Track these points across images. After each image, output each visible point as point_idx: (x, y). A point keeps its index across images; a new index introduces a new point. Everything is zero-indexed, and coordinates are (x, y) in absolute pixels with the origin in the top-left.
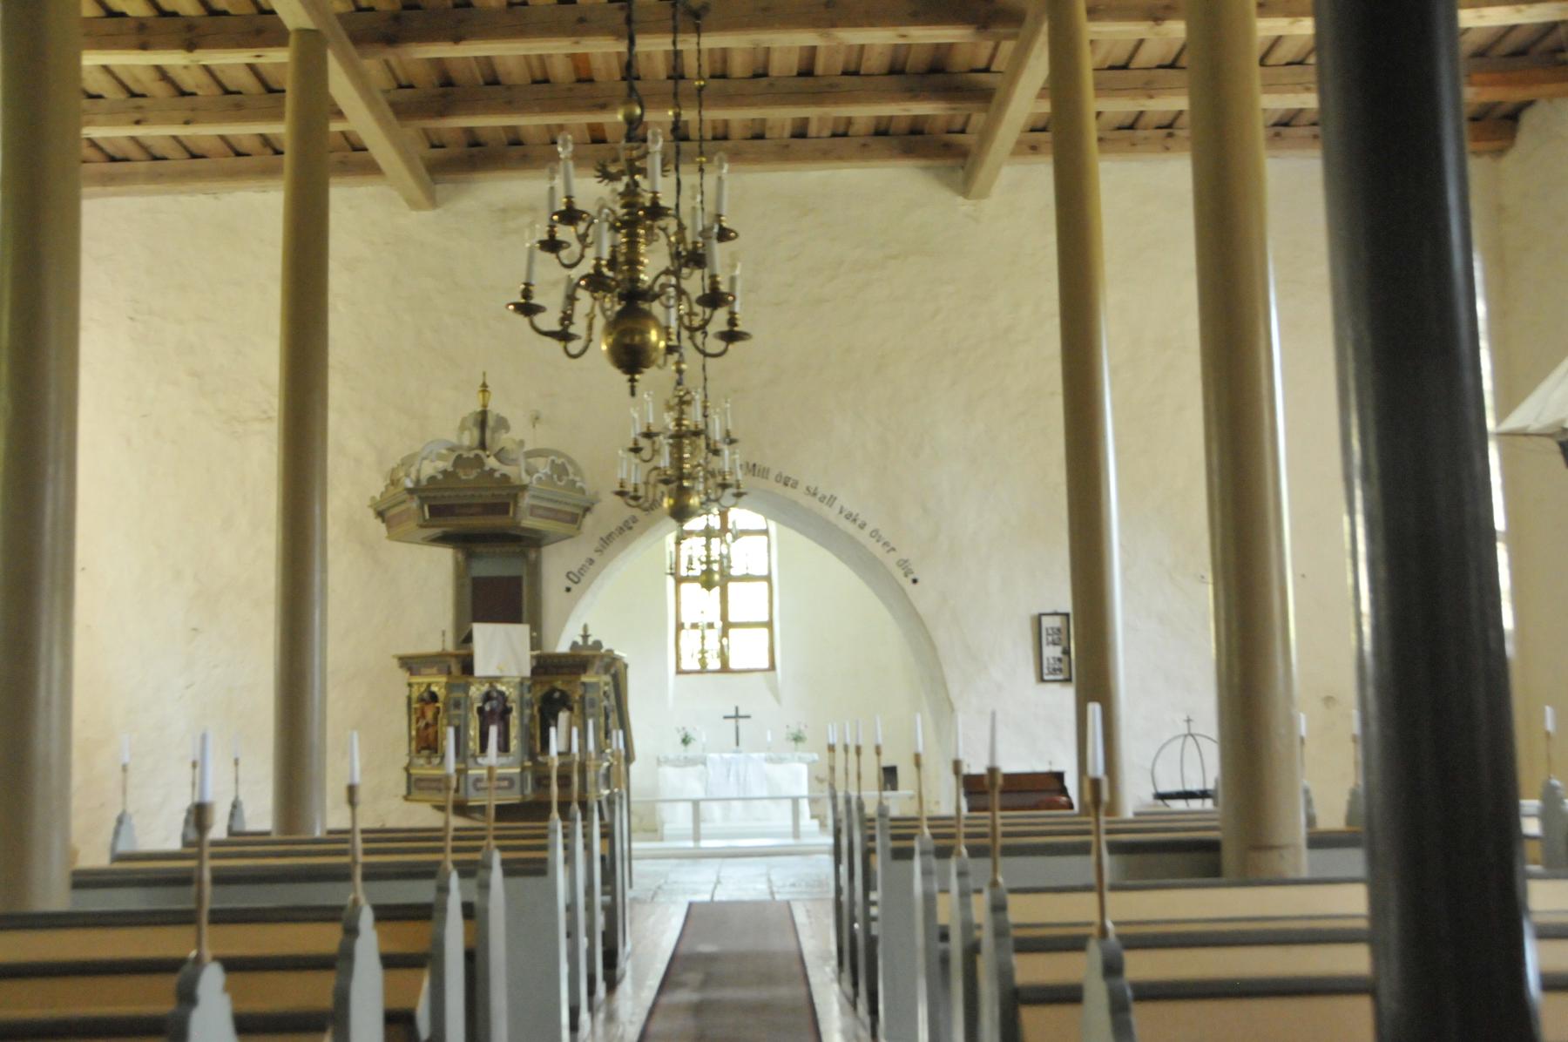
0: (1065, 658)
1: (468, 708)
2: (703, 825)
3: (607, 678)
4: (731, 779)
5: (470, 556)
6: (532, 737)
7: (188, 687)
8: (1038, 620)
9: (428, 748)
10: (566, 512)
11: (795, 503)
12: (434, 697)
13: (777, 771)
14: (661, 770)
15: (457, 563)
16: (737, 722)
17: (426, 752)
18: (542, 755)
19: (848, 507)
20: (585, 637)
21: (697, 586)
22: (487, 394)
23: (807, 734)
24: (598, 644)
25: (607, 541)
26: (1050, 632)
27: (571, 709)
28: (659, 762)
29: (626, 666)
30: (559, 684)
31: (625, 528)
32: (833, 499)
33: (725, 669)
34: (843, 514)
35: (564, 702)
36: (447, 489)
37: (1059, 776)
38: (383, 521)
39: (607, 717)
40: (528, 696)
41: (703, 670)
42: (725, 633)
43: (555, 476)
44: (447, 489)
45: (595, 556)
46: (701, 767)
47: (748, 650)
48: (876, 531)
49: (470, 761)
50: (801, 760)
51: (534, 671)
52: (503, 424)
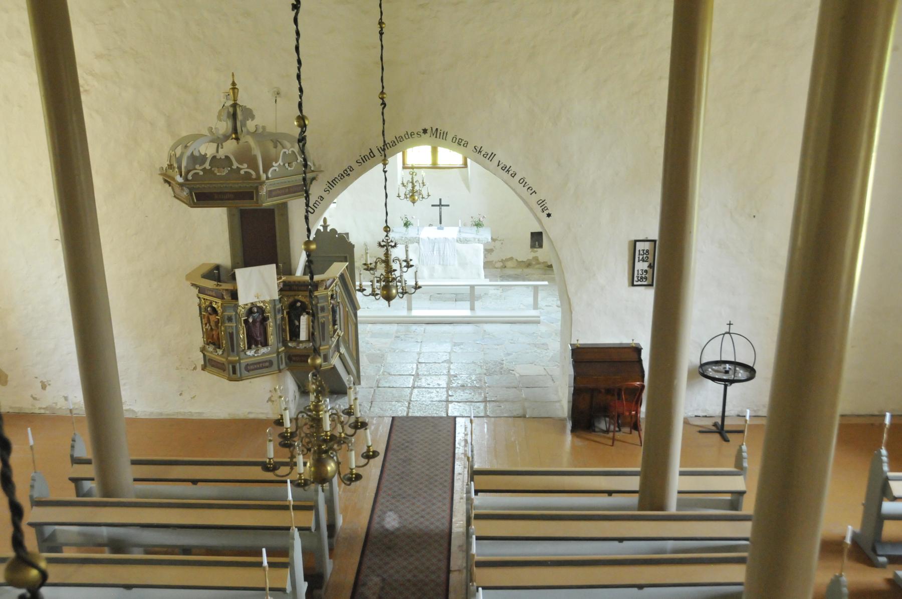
0: (650, 271)
1: (238, 321)
4: (435, 252)
6: (284, 330)
7: (59, 277)
9: (214, 344)
12: (215, 311)
16: (440, 209)
22: (236, 90)
23: (484, 222)
24: (334, 231)
25: (332, 184)
26: (641, 252)
31: (345, 175)
32: (493, 155)
34: (500, 167)
35: (304, 309)
37: (638, 350)
43: (287, 165)
45: (324, 194)
48: (523, 179)
49: (242, 354)
52: (249, 114)
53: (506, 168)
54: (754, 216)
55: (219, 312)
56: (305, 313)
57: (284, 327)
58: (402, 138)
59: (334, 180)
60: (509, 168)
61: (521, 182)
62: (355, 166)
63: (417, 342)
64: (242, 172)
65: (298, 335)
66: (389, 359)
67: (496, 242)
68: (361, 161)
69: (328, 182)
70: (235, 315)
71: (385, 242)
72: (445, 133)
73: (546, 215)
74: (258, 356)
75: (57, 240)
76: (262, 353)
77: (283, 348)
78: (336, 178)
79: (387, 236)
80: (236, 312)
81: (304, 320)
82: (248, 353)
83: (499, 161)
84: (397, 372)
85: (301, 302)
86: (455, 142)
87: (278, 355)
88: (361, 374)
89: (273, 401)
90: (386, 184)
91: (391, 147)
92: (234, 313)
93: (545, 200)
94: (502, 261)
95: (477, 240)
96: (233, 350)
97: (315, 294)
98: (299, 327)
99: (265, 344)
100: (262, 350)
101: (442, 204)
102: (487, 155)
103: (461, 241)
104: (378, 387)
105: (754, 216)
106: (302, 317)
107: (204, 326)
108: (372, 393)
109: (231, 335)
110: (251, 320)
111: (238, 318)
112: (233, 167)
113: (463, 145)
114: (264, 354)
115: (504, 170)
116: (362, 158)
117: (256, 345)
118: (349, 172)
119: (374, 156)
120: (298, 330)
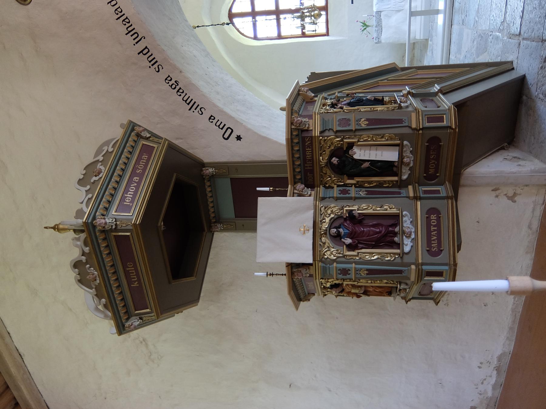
5: (219, 220)
6: (380, 185)
14: (383, 41)
18: (401, 176)
25: (191, 104)
27: (351, 146)
28: (379, 42)
30: (323, 160)
31: (178, 88)
39: (360, 102)
40: (336, 192)
45: (206, 115)
46: (382, 14)
49: (406, 259)
51: (311, 185)
57: (375, 184)
58: (116, 10)
59: (186, 101)
62: (163, 75)
65: (390, 164)
66: (484, 26)
68: (156, 65)
69: (190, 110)
74: (416, 232)
75: (290, 386)
76: (411, 226)
77: (410, 187)
78: (183, 99)
80: (334, 261)
81: (359, 154)
82: (407, 249)
85: (331, 157)
87: (420, 198)
88: (499, 60)
89: (515, 194)
91: (131, 25)
92: (335, 264)
96: (400, 272)
97: (317, 133)
98: (373, 162)
99: (396, 219)
100: (405, 225)
106: (356, 157)
108: (529, 42)
109: (371, 272)
110: (348, 241)
111: (343, 259)
112: (84, 261)
114: (414, 222)
116: (152, 65)
117: (395, 234)
118: (173, 82)
119: (146, 48)
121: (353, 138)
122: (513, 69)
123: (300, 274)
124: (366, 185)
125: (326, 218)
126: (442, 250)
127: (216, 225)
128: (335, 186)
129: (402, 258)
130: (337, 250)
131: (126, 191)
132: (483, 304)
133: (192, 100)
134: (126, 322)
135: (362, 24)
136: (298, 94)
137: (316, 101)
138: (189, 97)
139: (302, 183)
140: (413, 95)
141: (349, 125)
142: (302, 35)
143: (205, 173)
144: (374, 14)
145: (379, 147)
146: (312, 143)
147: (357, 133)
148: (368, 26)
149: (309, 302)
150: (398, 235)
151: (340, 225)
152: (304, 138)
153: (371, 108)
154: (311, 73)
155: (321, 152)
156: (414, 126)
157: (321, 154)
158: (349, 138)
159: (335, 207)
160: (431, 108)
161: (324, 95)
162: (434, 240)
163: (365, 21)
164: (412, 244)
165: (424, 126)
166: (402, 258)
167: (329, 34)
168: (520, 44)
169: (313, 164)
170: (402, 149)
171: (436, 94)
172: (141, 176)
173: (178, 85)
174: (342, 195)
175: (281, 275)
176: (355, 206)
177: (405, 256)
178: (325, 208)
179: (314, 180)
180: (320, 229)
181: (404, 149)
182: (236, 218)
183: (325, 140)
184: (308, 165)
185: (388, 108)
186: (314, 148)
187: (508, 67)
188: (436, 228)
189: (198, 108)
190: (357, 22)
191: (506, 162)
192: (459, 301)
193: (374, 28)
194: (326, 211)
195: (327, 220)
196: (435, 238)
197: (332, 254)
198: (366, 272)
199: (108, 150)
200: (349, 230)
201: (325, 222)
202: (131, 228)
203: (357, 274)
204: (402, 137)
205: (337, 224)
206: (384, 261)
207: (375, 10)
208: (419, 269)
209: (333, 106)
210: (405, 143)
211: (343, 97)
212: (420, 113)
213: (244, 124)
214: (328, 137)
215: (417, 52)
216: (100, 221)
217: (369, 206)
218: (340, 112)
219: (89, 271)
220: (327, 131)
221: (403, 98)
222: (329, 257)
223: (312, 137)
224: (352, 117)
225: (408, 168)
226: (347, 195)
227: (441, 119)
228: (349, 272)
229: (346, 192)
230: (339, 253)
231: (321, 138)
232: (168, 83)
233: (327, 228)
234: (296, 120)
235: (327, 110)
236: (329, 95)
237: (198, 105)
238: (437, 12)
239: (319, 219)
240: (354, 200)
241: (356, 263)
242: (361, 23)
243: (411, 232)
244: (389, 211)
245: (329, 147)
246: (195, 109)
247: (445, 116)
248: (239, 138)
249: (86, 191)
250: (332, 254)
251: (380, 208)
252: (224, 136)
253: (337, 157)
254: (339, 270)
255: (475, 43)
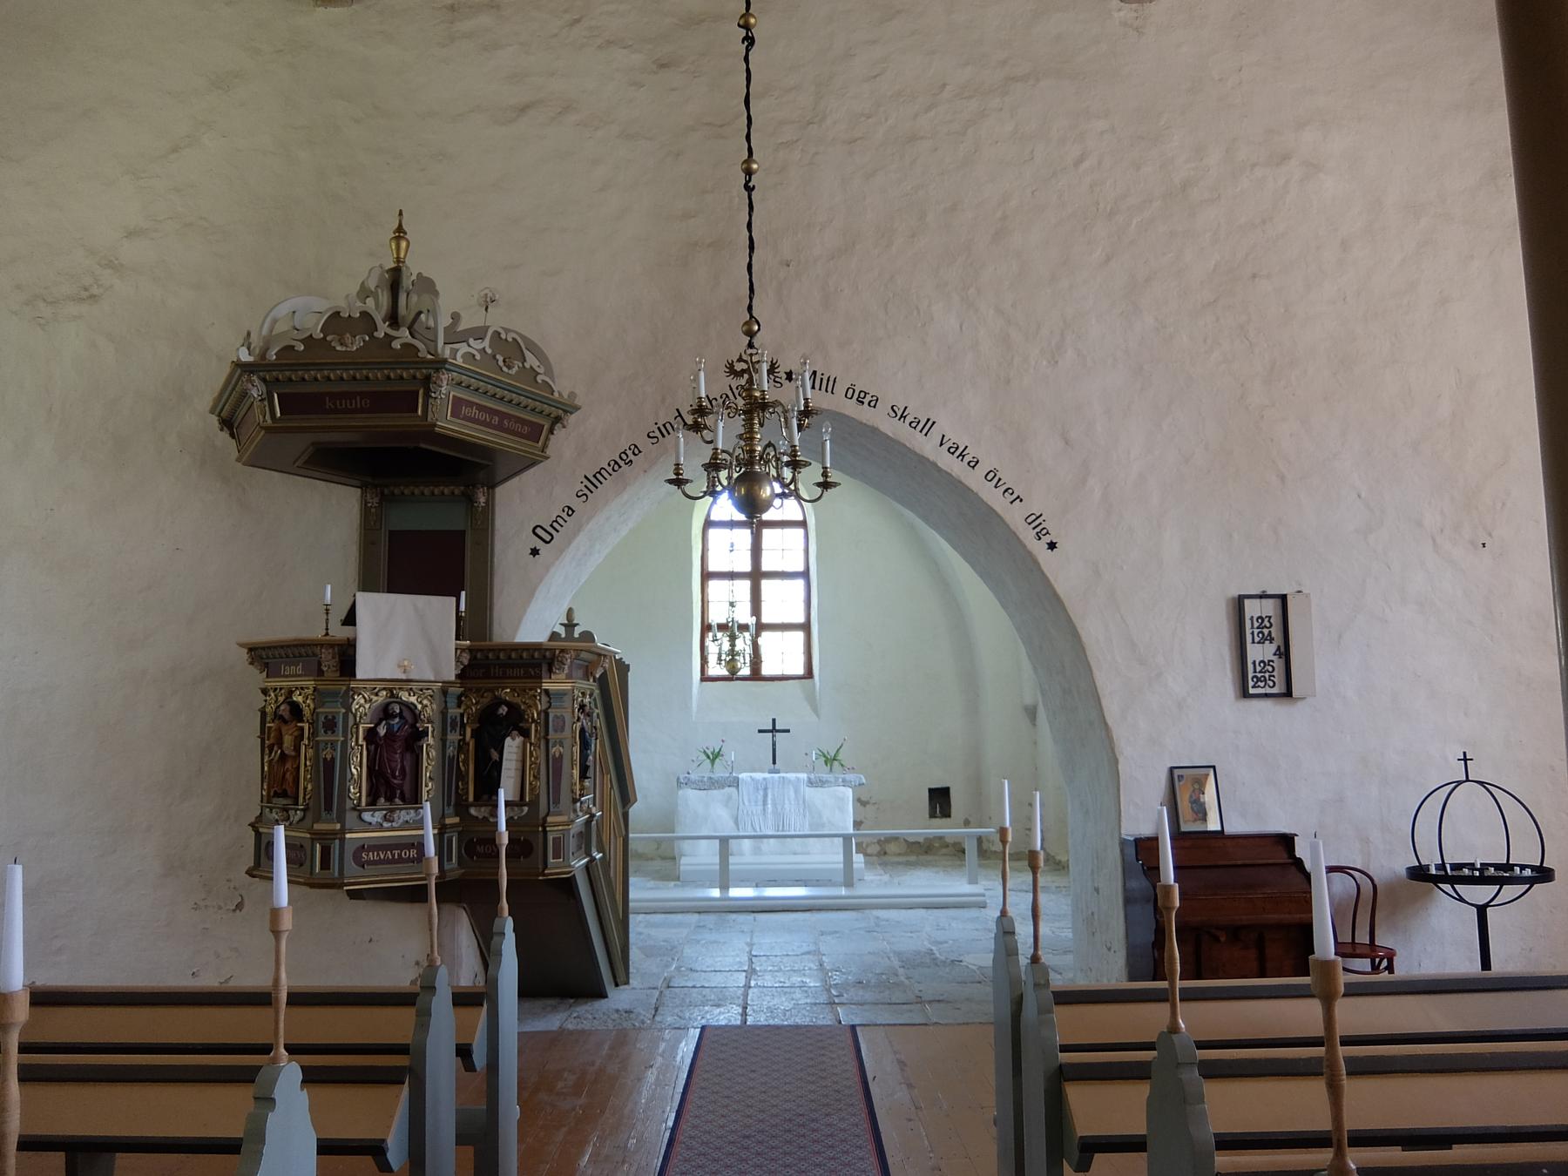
2: (732, 860)
3: (590, 685)
5: (384, 499)
6: (462, 777)
8: (1239, 603)
9: (284, 795)
10: (523, 422)
11: (875, 431)
12: (296, 710)
13: (815, 795)
14: (680, 792)
15: (365, 511)
17: (282, 801)
19: (954, 437)
20: (570, 626)
21: (744, 35)
24: (588, 636)
25: (593, 481)
27: (525, 734)
29: (623, 669)
30: (506, 693)
31: (622, 463)
32: (930, 424)
33: (756, 675)
34: (945, 447)
35: (516, 722)
36: (307, 366)
38: (232, 435)
39: (585, 745)
40: (454, 711)
41: (733, 676)
42: (758, 634)
44: (307, 366)
45: (575, 503)
46: (733, 790)
47: (783, 654)
48: (994, 472)
49: (351, 817)
50: (845, 783)
52: (427, 285)
53: (957, 448)
54: (1484, 545)
55: (307, 712)
56: (515, 733)
57: (463, 769)
59: (599, 473)
60: (963, 451)
61: (989, 477)
62: (644, 443)
63: (743, 932)
64: (396, 345)
67: (868, 806)
68: (657, 434)
69: (586, 477)
70: (346, 716)
71: (746, 362)
72: (832, 379)
73: (1047, 546)
76: (401, 821)
77: (457, 820)
78: (602, 468)
79: (751, 345)
80: (349, 709)
81: (512, 745)
82: (367, 816)
83: (943, 436)
84: (708, 967)
85: (508, 704)
86: (851, 398)
90: (750, 216)
93: (1041, 515)
94: (879, 842)
95: (840, 780)
96: (329, 808)
97: (545, 686)
98: (499, 764)
100: (403, 812)
101: (777, 728)
102: (919, 422)
103: (812, 784)
104: (669, 987)
105: (1484, 545)
106: (508, 740)
107: (267, 751)
109: (329, 765)
110: (382, 731)
112: (376, 334)
113: (869, 404)
115: (953, 453)
116: (659, 428)
117: (390, 799)
118: (631, 457)
120: (496, 774)
121: (535, 736)
122: (617, 985)
123: (330, 657)
124: (463, 756)
125: (416, 697)
126: (363, 867)
127: (377, 496)
128: (461, 711)
129: (354, 809)
130: (366, 714)
131: (481, 408)
132: (198, 971)
133: (601, 483)
134: (259, 377)
135: (717, 750)
136: (600, 655)
137: (589, 680)
138: (606, 479)
139: (470, 660)
140: (588, 823)
141: (556, 731)
142: (706, 623)
143: (478, 491)
144: (734, 775)
145: (519, 773)
146: (531, 677)
147: (543, 742)
148: (713, 761)
149: (247, 663)
150: (388, 804)
151: (404, 718)
152: (540, 666)
153: (576, 760)
154: (628, 665)
155: (517, 690)
156: (549, 819)
157: (515, 690)
158: (536, 731)
159: (433, 711)
160: (572, 844)
161: (597, 692)
162: (378, 854)
163: (722, 755)
164: (374, 823)
165: (549, 833)
166: (354, 809)
167: (704, 683)
168: (654, 988)
169: (499, 678)
170: (517, 805)
171: (588, 854)
172: (500, 427)
173: (626, 464)
174: (449, 721)
175: (327, 626)
176: (434, 741)
177: (356, 813)
178: (431, 696)
179: (474, 678)
180: (400, 688)
181: (516, 808)
182: (392, 533)
183: (535, 697)
184: (497, 671)
185: (576, 784)
186: (524, 681)
187: (621, 979)
188: (396, 857)
189: (586, 491)
190: (723, 741)
191: (473, 976)
192: (204, 928)
193: (707, 775)
194: (426, 698)
195: (413, 699)
196: (382, 857)
197: (360, 707)
198: (329, 757)
199: (539, 374)
200: (397, 732)
201: (410, 695)
202: (429, 419)
203: (327, 744)
204: (534, 804)
205: (407, 714)
206: (348, 784)
207: (743, 776)
208: (336, 834)
209: (582, 707)
210: (526, 809)
211: (591, 721)
212: (566, 827)
213: (557, 563)
214: (540, 700)
215: (657, 865)
216: (445, 377)
217: (432, 761)
218: (574, 717)
219: (357, 337)
220: (548, 699)
221: (586, 805)
222: (355, 702)
223: (541, 678)
224: (567, 732)
225: (486, 815)
226: (449, 729)
227: (556, 856)
228: (329, 732)
229: (453, 728)
230: (361, 717)
231: (539, 691)
232: (630, 449)
233: (401, 698)
234: (567, 656)
235: (577, 699)
236: (595, 700)
237: (592, 492)
238: (724, 887)
239: (414, 686)
240: (441, 739)
241: (344, 743)
242: (720, 750)
243: (393, 821)
244: (425, 790)
245: (524, 703)
246: (586, 486)
247: (561, 860)
248: (535, 552)
249: (484, 349)
250: (360, 707)
251: (430, 777)
252: (548, 540)
253: (507, 713)
254: (334, 718)
255: (662, 943)
